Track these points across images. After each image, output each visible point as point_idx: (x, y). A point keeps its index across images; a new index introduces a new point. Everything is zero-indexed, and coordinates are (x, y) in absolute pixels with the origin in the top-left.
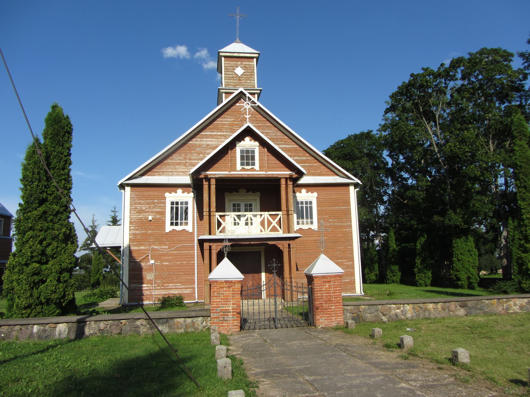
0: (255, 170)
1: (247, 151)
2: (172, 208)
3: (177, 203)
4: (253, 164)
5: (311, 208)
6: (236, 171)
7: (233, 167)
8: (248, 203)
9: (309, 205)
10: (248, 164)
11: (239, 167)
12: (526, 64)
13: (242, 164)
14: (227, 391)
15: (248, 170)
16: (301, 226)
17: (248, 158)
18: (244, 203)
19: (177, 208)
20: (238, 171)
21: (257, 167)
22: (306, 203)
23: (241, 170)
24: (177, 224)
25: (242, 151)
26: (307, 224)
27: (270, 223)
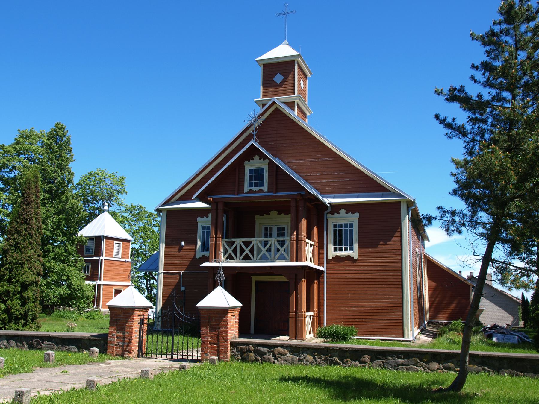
0: (263, 192)
1: (256, 171)
2: (335, 232)
3: (341, 226)
4: (262, 185)
5: (351, 231)
6: (243, 193)
7: (241, 190)
8: (281, 227)
9: (338, 229)
10: (256, 185)
11: (247, 189)
12: (504, 26)
13: (250, 185)
14: (86, 388)
15: (256, 192)
16: (338, 253)
17: (256, 177)
18: (276, 227)
19: (341, 231)
20: (246, 193)
21: (265, 188)
22: (346, 226)
23: (249, 193)
24: (341, 250)
25: (251, 171)
26: (346, 249)
27: (242, 251)
